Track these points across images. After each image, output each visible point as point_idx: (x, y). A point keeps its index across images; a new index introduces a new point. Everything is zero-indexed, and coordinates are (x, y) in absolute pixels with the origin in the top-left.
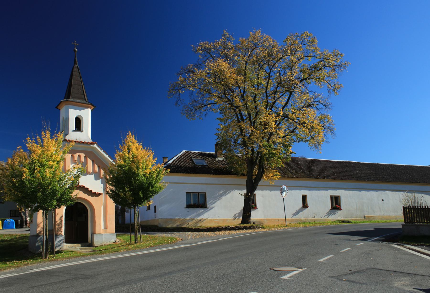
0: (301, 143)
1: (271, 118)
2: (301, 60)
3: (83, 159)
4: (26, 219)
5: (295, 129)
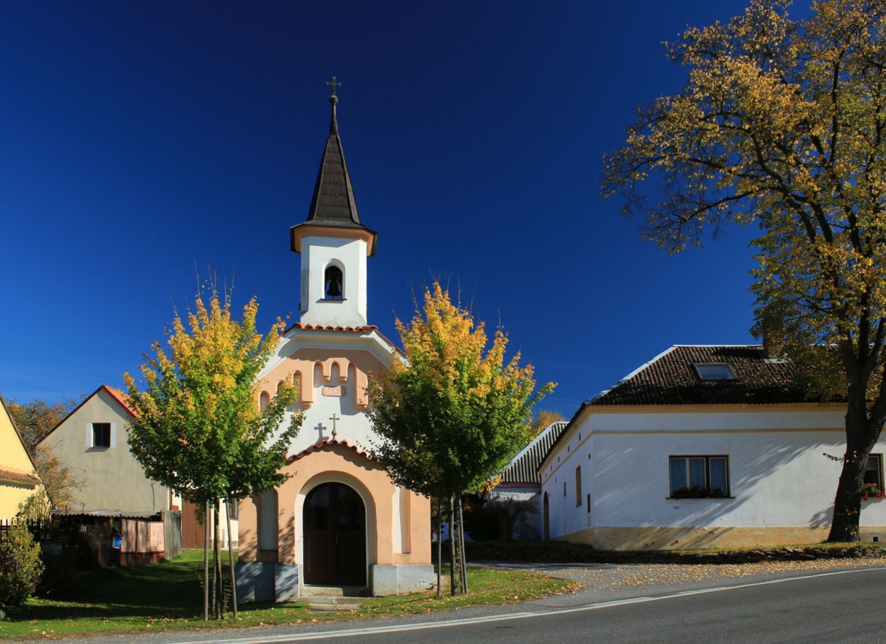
3: (344, 372)
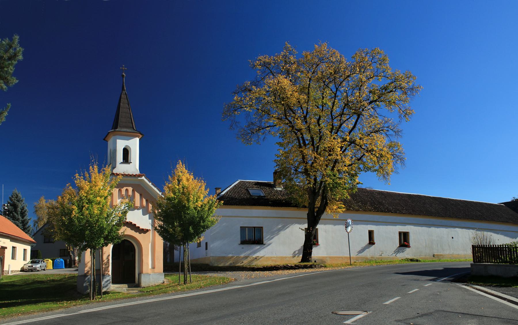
0: (369, 173)
1: (337, 144)
2: (371, 80)
3: (130, 193)
4: (74, 258)
5: (362, 156)
